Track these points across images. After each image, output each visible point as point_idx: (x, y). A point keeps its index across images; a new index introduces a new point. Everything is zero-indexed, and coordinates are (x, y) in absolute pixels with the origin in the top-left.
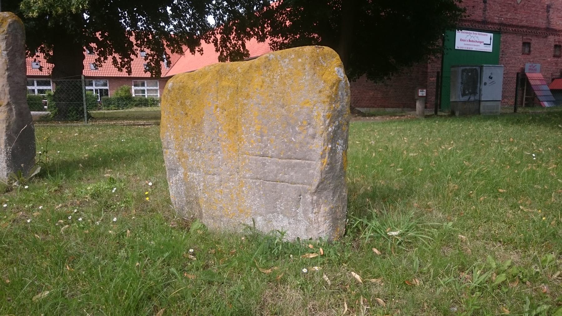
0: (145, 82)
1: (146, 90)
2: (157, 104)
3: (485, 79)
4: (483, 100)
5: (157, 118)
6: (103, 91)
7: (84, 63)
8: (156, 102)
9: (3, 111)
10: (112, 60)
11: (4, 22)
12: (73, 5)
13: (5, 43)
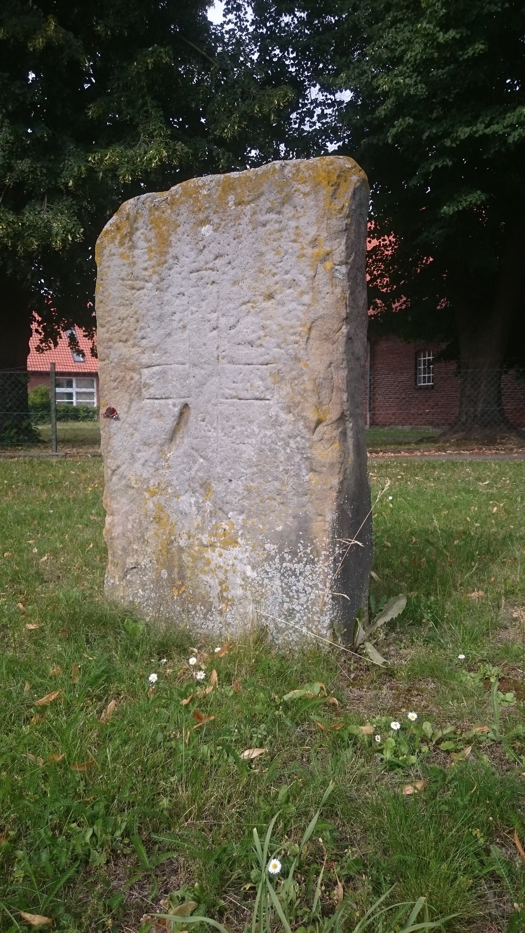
0: (74, 379)
1: (74, 394)
2: (92, 417)
5: (95, 441)
6: (65, 385)
7: (30, 344)
8: (91, 413)
9: (326, 437)
10: (68, 340)
11: (343, 184)
12: (57, 235)
13: (344, 241)
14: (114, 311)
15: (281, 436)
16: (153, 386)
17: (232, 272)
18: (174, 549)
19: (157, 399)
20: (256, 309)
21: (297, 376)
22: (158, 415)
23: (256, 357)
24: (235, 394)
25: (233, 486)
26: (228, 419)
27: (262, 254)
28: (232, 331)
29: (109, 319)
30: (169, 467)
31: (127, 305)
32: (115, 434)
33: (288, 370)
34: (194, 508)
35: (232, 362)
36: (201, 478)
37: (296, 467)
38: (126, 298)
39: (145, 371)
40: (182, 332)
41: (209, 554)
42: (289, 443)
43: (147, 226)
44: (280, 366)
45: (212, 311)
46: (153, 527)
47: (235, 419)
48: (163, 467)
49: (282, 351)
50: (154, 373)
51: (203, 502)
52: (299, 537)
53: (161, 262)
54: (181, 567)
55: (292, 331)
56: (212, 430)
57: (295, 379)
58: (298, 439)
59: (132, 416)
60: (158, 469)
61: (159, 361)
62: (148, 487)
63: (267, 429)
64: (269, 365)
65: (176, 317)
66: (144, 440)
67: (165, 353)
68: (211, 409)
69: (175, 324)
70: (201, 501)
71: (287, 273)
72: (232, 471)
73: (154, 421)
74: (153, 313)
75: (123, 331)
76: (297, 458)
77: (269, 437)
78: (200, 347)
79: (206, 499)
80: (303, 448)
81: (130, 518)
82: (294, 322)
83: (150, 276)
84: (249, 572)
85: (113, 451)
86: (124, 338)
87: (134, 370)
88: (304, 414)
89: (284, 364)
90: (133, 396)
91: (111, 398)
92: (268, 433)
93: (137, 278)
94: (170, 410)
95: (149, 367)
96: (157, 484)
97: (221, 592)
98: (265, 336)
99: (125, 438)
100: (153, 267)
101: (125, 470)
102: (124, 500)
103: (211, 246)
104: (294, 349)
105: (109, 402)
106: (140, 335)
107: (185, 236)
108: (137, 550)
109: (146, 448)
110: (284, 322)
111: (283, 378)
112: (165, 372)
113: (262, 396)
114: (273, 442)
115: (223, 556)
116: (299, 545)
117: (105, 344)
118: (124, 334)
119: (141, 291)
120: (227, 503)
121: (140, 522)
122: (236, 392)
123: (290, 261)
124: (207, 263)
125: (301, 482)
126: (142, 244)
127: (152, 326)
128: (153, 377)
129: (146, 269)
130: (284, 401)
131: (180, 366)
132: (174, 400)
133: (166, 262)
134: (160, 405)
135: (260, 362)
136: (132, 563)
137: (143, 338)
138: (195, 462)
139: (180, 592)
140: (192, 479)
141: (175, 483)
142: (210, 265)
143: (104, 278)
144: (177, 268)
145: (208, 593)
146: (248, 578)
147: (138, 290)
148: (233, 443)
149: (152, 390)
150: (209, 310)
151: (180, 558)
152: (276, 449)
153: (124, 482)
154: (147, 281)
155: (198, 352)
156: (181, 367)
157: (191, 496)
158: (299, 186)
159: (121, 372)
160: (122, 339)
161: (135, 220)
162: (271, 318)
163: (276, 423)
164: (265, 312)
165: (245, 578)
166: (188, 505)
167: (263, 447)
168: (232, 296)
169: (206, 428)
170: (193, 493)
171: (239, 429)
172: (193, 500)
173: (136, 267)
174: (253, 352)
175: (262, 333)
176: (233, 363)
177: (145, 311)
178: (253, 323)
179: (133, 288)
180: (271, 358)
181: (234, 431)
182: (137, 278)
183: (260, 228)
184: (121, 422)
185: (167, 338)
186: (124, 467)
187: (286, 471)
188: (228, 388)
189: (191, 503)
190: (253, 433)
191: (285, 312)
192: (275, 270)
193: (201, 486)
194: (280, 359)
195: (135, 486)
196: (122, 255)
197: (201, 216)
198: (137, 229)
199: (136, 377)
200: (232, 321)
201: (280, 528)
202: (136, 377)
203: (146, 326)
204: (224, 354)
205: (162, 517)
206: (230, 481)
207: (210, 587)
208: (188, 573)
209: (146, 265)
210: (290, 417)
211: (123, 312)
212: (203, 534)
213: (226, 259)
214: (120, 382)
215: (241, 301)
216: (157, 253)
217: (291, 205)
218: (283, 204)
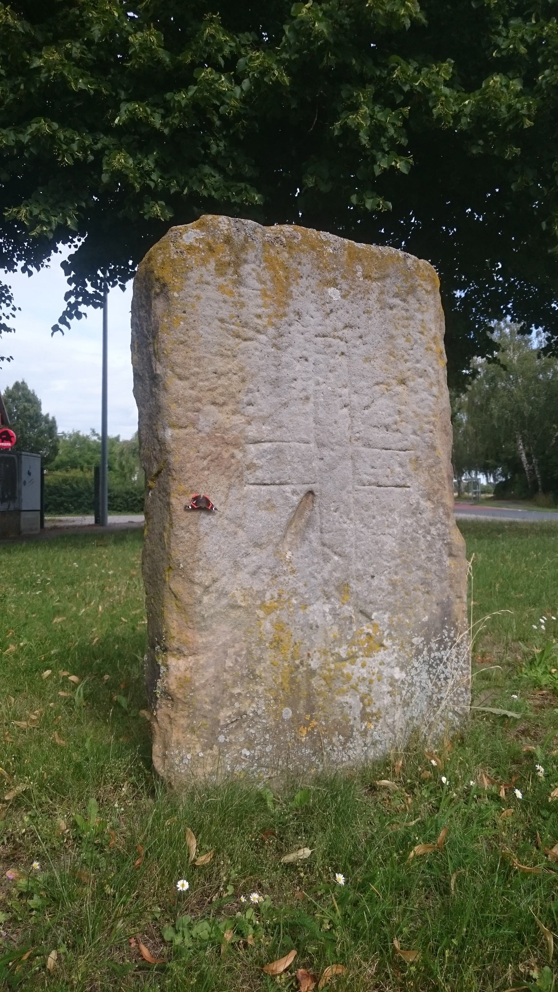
3: (24, 476)
4: (24, 508)
14: (206, 360)
15: (422, 524)
16: (261, 467)
17: (363, 348)
18: (300, 676)
19: (265, 484)
20: (391, 392)
21: (434, 464)
22: (268, 505)
23: (395, 442)
24: (374, 480)
25: (375, 582)
26: (367, 508)
27: (392, 337)
28: (366, 412)
29: (196, 369)
30: (293, 572)
31: (228, 357)
32: (206, 534)
33: (425, 457)
34: (329, 617)
35: (368, 445)
36: (338, 579)
37: (437, 553)
38: (228, 348)
39: (252, 448)
40: (303, 404)
41: (348, 668)
42: (430, 530)
43: (261, 263)
44: (419, 454)
45: (343, 386)
46: (269, 655)
47: (374, 508)
48: (285, 573)
49: (418, 438)
50: (265, 451)
51: (340, 608)
52: (443, 623)
53: (279, 314)
54: (310, 697)
55: (426, 419)
56: (348, 522)
57: (433, 466)
58: (439, 525)
59: (233, 508)
60: (276, 576)
61: (271, 437)
62: (263, 602)
63: (407, 517)
64: (407, 452)
65: (298, 384)
66: (255, 540)
67: (280, 427)
68: (346, 497)
69: (294, 393)
70: (337, 607)
71: (418, 361)
72: (374, 566)
73: (263, 513)
74: (265, 374)
75: (220, 390)
76: (439, 544)
77: (410, 526)
78: (330, 425)
79: (343, 604)
80: (444, 534)
81: (231, 651)
82: (426, 410)
83: (265, 327)
84: (398, 674)
85: (204, 559)
86: (221, 400)
87: (236, 445)
88: (444, 501)
89: (422, 451)
90: (233, 480)
91: (198, 483)
92: (409, 521)
93: (245, 325)
94: (287, 498)
95: (256, 442)
96: (276, 596)
97: (364, 709)
98: (401, 421)
99: (223, 539)
100: (269, 316)
101: (227, 583)
102: (225, 627)
103: (339, 312)
104: (430, 438)
105: (195, 488)
106: (246, 399)
107: (309, 291)
108: (239, 694)
109: (258, 550)
110: (419, 410)
111: (421, 465)
112: (281, 451)
113: (403, 483)
114: (414, 531)
115: (367, 665)
116: (444, 631)
117: (189, 405)
118: (222, 394)
119: (248, 343)
120: (371, 603)
121: (250, 653)
122: (376, 478)
123: (419, 352)
124: (335, 330)
125: (443, 567)
126: (252, 282)
127: (263, 390)
128: (263, 456)
129: (259, 316)
130: (424, 488)
131: (302, 444)
132: (293, 487)
133: (285, 315)
134: (271, 492)
135: (399, 447)
136: (229, 717)
137: (250, 404)
138: (326, 559)
139: (309, 729)
140: (326, 582)
141: (302, 590)
142: (340, 334)
143: (188, 310)
144: (297, 326)
145: (345, 717)
146: (397, 681)
147: (245, 340)
148: (374, 534)
149: (259, 474)
150: (339, 384)
151: (309, 685)
152: (418, 538)
153: (224, 602)
154: (258, 332)
155: (329, 431)
156: (303, 446)
157: (324, 603)
158: (422, 282)
159: (216, 446)
160: (217, 401)
161: (243, 248)
162: (406, 403)
163: (416, 511)
164: (399, 396)
165: (392, 682)
166: (321, 614)
167: (405, 536)
168: (365, 373)
169: (341, 520)
170: (328, 599)
171: (379, 518)
172: (327, 608)
173: (245, 309)
174: (392, 437)
175: (397, 417)
176: (370, 446)
177: (253, 371)
178: (388, 406)
179: (238, 337)
180: (410, 444)
181: (374, 521)
182: (245, 325)
183: (387, 309)
184: (215, 517)
185: (282, 409)
186: (224, 579)
187: (429, 559)
188: (365, 474)
189: (324, 612)
190: (395, 524)
191: (418, 400)
192: (406, 357)
193: (337, 588)
194: (418, 446)
195: (243, 604)
196: (220, 288)
197: (329, 276)
198: (246, 261)
199: (239, 455)
200: (366, 400)
201: (426, 619)
202: (239, 455)
203: (255, 388)
204: (358, 435)
205: (282, 638)
206: (373, 577)
207: (351, 707)
208: (320, 701)
209: (259, 311)
210: (429, 504)
211: (220, 364)
212: (340, 647)
213: (358, 332)
214: (212, 461)
215: (374, 381)
216: (274, 301)
217: (414, 297)
218: (408, 293)
